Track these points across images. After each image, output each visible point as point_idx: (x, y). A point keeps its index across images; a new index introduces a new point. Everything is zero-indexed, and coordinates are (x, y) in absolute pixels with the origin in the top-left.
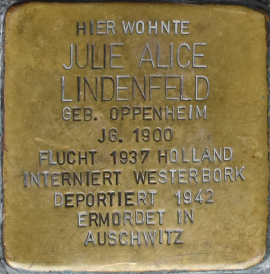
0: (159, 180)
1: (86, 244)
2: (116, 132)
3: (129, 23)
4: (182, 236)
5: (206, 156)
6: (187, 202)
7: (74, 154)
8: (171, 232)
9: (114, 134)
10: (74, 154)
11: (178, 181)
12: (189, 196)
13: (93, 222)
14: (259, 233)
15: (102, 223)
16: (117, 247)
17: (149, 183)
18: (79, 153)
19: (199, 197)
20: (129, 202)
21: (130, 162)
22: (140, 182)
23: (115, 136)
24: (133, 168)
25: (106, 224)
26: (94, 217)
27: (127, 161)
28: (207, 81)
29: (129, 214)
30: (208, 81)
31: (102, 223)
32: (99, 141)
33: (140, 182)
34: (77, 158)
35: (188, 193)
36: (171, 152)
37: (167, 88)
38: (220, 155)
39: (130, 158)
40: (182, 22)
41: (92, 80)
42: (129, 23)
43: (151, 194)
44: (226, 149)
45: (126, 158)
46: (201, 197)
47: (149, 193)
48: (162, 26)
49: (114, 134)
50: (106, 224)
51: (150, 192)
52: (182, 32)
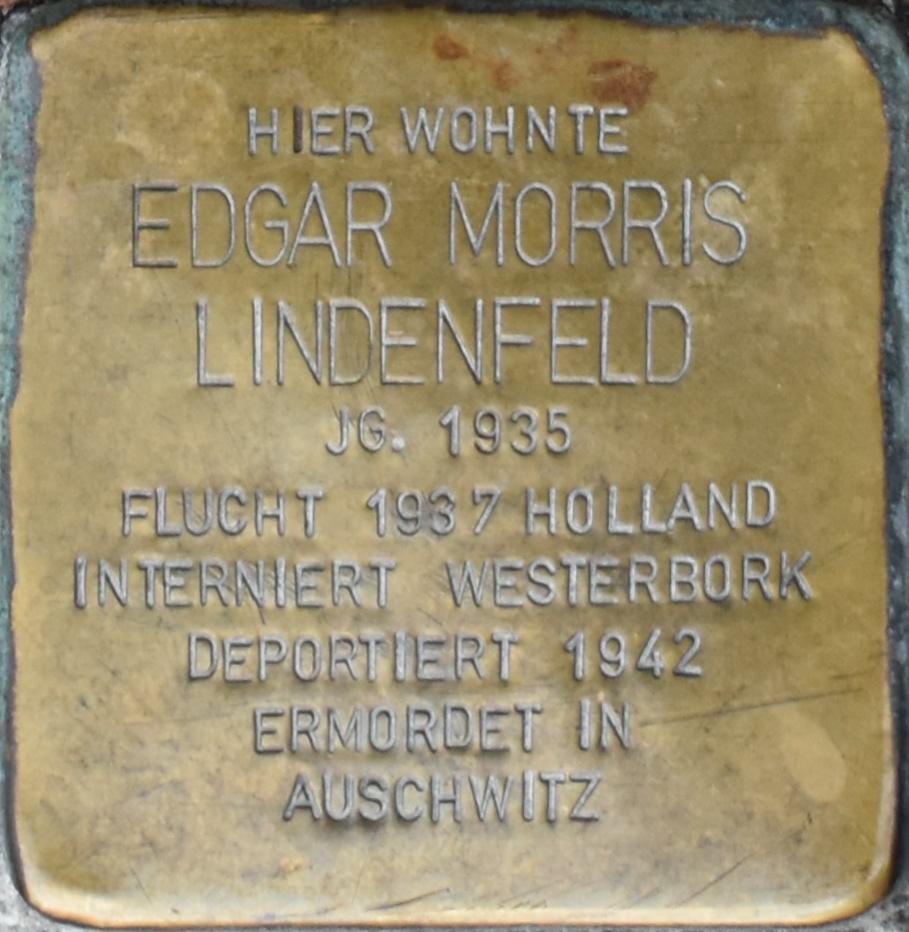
0: (532, 593)
1: (289, 814)
3: (423, 114)
4: (723, 719)
6: (609, 670)
8: (558, 782)
12: (618, 652)
16: (391, 829)
19: (652, 656)
28: (228, 204)
29: (426, 713)
30: (231, 202)
35: (615, 641)
38: (730, 504)
40: (603, 113)
41: (859, 347)
42: (423, 114)
43: (499, 643)
44: (757, 489)
46: (657, 654)
47: (493, 641)
48: (553, 132)
51: (496, 638)
52: (602, 146)
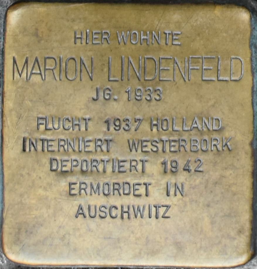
2: (110, 90)
5: (195, 126)
7: (116, 208)
9: (109, 92)
10: (116, 208)
11: (144, 78)
13: (83, 191)
14: (248, 191)
15: (93, 193)
17: (142, 151)
18: (122, 207)
20: (121, 169)
21: (124, 129)
22: (134, 150)
23: (109, 94)
24: (127, 136)
25: (97, 193)
26: (62, 143)
27: (120, 128)
31: (93, 193)
32: (94, 99)
33: (134, 150)
34: (119, 212)
36: (132, 33)
37: (160, 69)
39: (123, 125)
45: (120, 126)
49: (109, 92)
50: (97, 193)
